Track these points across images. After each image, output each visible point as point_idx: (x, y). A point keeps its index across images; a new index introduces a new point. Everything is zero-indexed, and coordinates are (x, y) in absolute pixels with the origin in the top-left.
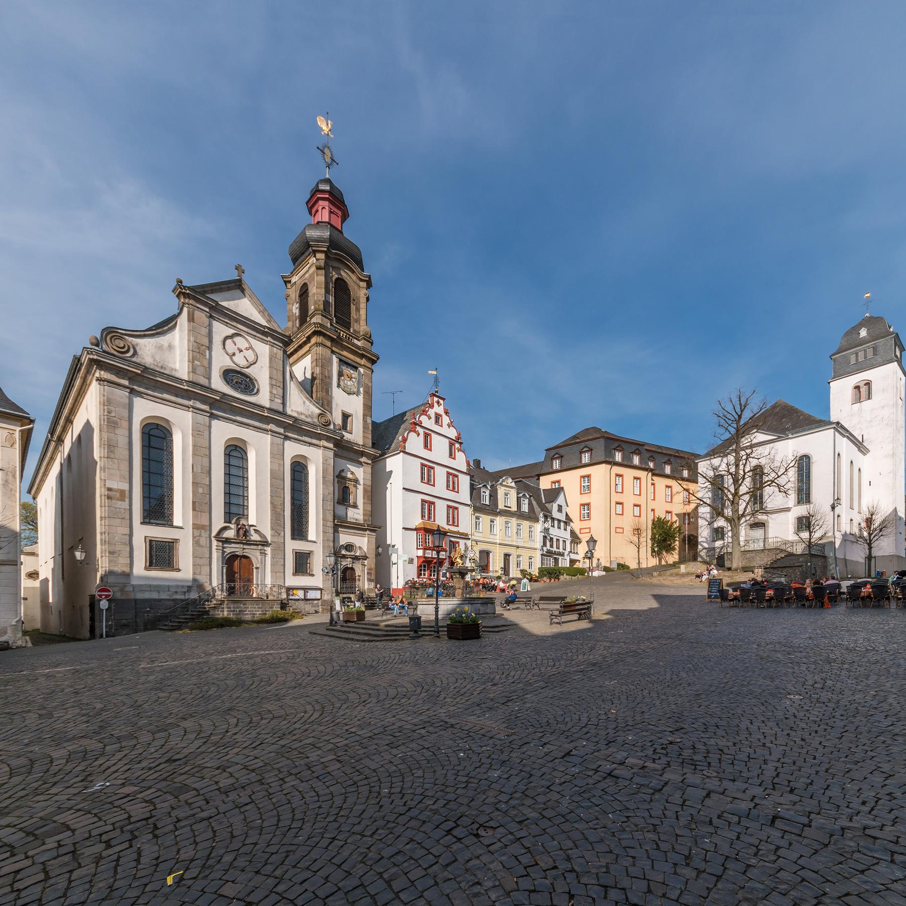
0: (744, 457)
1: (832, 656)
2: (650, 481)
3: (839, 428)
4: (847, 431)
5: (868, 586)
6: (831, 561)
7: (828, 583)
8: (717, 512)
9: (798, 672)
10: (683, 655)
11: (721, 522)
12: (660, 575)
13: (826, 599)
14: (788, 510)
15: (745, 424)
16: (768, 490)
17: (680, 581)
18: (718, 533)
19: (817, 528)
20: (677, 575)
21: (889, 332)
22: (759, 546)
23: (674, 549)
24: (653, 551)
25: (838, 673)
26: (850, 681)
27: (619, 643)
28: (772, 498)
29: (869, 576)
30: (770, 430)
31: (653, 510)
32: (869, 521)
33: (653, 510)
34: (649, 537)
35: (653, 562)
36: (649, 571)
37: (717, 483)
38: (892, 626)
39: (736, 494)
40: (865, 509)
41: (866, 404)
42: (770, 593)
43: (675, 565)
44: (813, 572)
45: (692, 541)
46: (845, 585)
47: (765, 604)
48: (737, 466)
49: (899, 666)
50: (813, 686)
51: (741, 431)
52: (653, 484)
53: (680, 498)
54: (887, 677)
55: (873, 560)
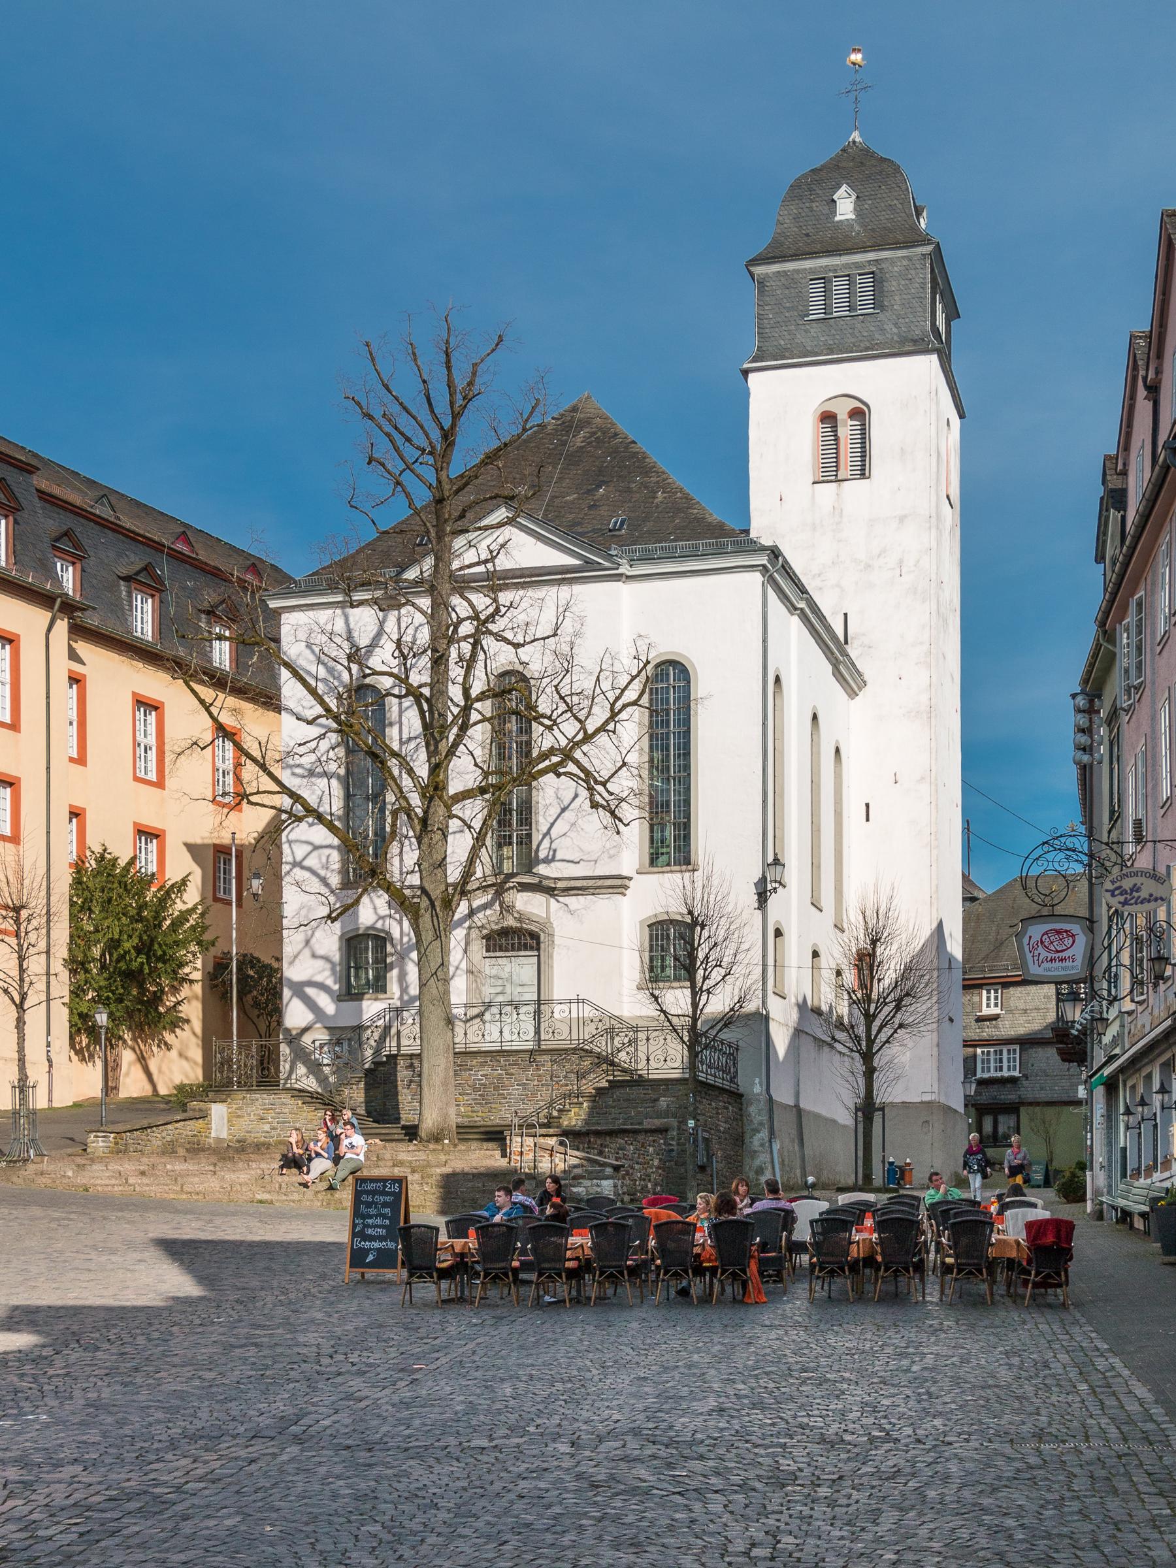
0: (466, 628)
1: (786, 1464)
2: (61, 665)
3: (778, 571)
4: (803, 591)
5: (869, 1222)
6: (756, 1113)
7: (760, 1206)
8: (364, 869)
9: (703, 1519)
10: (335, 1496)
11: (373, 910)
12: (120, 1151)
13: (753, 1267)
14: (616, 884)
15: (465, 481)
16: (551, 792)
17: (212, 1184)
18: (364, 961)
19: (717, 975)
20: (196, 1149)
21: (915, 228)
22: (515, 1032)
23: (177, 1023)
24: (82, 1024)
25: (806, 1511)
26: (836, 1533)
27: (58, 1465)
28: (572, 830)
29: (866, 1184)
30: (558, 523)
31: (76, 814)
32: (866, 962)
33: (76, 814)
34: (61, 951)
35: (75, 1082)
36: (71, 1129)
37: (357, 714)
38: (929, 1360)
39: (434, 789)
40: (853, 917)
41: (854, 489)
42: (580, 1241)
43: (185, 1102)
44: (701, 1159)
45: (250, 992)
46: (808, 1211)
47: (562, 1289)
48: (439, 662)
49: (947, 1478)
50: (747, 1554)
51: (453, 507)
52: (75, 680)
53: (195, 774)
54: (920, 1514)
55: (878, 1117)
